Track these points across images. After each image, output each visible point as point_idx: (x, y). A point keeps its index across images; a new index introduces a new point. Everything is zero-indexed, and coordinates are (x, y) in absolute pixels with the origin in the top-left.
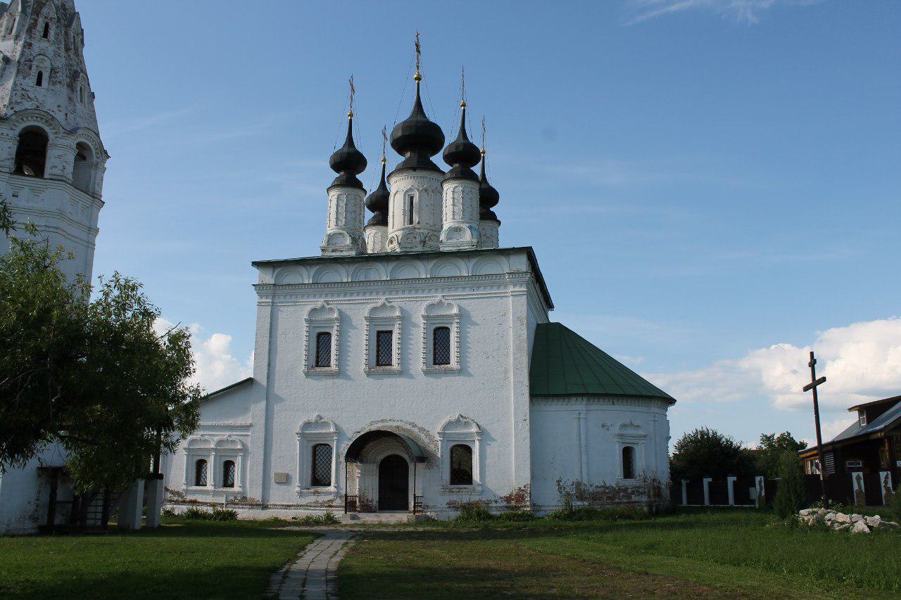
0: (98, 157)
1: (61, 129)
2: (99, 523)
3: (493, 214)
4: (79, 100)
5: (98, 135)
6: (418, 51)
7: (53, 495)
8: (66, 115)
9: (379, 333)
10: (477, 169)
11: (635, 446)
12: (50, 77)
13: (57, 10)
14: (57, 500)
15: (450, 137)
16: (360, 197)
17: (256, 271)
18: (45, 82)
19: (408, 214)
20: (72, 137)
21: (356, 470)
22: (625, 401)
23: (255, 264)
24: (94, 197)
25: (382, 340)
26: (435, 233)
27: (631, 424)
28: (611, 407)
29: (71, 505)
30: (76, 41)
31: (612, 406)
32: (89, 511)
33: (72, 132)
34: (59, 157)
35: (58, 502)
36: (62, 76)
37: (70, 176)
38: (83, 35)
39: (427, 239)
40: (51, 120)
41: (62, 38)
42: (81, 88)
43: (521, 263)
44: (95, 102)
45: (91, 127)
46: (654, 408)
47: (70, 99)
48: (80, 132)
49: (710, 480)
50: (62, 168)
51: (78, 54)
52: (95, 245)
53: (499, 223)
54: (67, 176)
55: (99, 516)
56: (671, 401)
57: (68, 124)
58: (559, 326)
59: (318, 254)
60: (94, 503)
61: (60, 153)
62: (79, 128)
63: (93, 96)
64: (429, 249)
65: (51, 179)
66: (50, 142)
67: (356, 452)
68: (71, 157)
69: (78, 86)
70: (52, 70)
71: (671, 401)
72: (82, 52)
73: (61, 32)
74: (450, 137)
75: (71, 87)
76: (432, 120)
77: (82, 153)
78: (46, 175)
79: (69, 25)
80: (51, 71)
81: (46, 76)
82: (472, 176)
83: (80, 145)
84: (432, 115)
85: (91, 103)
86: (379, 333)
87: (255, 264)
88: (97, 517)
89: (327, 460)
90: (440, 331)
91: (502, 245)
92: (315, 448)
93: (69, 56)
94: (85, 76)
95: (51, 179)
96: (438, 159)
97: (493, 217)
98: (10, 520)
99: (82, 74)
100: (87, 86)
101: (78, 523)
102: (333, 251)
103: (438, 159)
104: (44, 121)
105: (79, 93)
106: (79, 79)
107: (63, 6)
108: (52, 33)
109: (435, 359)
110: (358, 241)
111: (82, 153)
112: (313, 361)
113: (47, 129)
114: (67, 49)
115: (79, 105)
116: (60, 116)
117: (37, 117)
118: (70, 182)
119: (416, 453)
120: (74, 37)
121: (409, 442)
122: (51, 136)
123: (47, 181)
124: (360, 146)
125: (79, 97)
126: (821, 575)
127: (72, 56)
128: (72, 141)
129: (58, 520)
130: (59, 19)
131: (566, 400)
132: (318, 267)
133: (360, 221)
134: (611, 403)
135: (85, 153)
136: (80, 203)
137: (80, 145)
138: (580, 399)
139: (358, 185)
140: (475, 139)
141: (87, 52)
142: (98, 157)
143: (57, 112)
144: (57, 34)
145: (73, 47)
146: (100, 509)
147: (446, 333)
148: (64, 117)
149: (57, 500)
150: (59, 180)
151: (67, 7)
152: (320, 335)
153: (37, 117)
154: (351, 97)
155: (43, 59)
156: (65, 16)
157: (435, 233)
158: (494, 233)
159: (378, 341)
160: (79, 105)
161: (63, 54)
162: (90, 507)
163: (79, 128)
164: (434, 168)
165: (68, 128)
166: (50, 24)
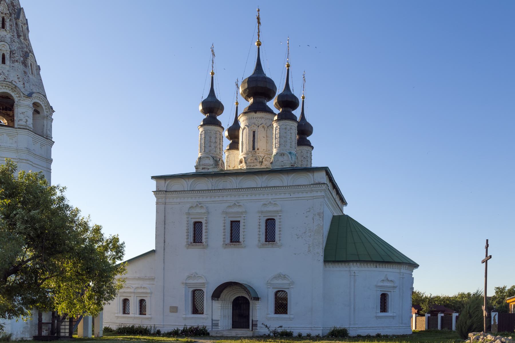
0: (47, 112)
1: (22, 94)
2: (67, 335)
3: (309, 141)
4: (31, 73)
5: (45, 96)
6: (259, 23)
7: (40, 319)
8: (24, 84)
9: (232, 222)
10: (297, 113)
11: (389, 293)
12: (10, 57)
13: (8, 7)
14: (42, 322)
15: (280, 90)
16: (220, 132)
17: (154, 182)
18: (7, 62)
19: (252, 143)
20: (29, 100)
21: (217, 305)
22: (384, 265)
23: (153, 178)
24: (47, 139)
25: (235, 226)
26: (269, 156)
27: (388, 280)
28: (375, 269)
29: (51, 325)
30: (24, 29)
31: (375, 268)
32: (61, 328)
33: (30, 95)
34: (23, 113)
35: (43, 323)
36: (18, 56)
37: (31, 126)
38: (27, 24)
39: (264, 160)
40: (15, 88)
41: (14, 28)
42: (31, 64)
43: (322, 177)
44: (41, 73)
45: (41, 91)
46: (404, 270)
47: (25, 72)
48: (34, 95)
49: (443, 315)
50: (25, 121)
51: (26, 39)
52: (51, 170)
53: (313, 148)
54: (30, 126)
55: (67, 331)
56: (416, 266)
57: (27, 90)
58: (347, 217)
59: (193, 170)
60: (63, 324)
61: (24, 110)
62: (33, 93)
63: (38, 68)
64: (265, 167)
65: (19, 128)
66: (16, 103)
67: (217, 295)
68: (30, 112)
69: (29, 61)
70: (11, 52)
71: (416, 266)
72: (28, 37)
73: (13, 24)
74: (280, 90)
75: (24, 63)
76: (268, 75)
77: (37, 109)
78: (16, 126)
79: (18, 18)
80: (10, 54)
81: (7, 56)
82: (293, 118)
83: (35, 104)
84: (269, 72)
85: (39, 74)
86: (232, 222)
87: (153, 178)
88: (66, 332)
89: (201, 302)
90: (270, 221)
91: (314, 165)
92: (194, 292)
93: (21, 41)
94: (33, 56)
95: (19, 128)
96: (272, 104)
97: (308, 144)
98: (17, 333)
99: (30, 54)
100: (34, 62)
101: (56, 335)
102: (203, 169)
103: (272, 104)
104: (10, 89)
105: (30, 67)
106: (29, 58)
107: (12, 3)
108: (7, 24)
109: (266, 239)
110: (217, 161)
111: (37, 109)
112: (191, 239)
113: (13, 94)
114: (19, 36)
115: (31, 76)
116: (20, 85)
117: (5, 86)
118: (32, 130)
119: (253, 295)
120: (22, 26)
121: (248, 288)
122: (16, 99)
123: (17, 129)
124: (220, 96)
125: (30, 70)
126: (319, 337)
127: (23, 41)
128: (29, 102)
129: (44, 333)
130: (11, 14)
131: (347, 264)
132: (193, 180)
133: (220, 148)
134: (375, 266)
135: (39, 109)
136: (39, 143)
137: (35, 104)
138: (355, 264)
139: (218, 124)
140: (297, 91)
141: (32, 37)
142: (47, 112)
143: (18, 82)
144: (11, 25)
145: (22, 35)
146: (68, 327)
147: (273, 222)
148: (22, 86)
149: (42, 322)
150: (24, 129)
151: (15, 4)
152: (195, 223)
153: (5, 86)
154: (213, 60)
155: (4, 44)
156: (15, 11)
157: (269, 156)
158: (309, 155)
159: (231, 227)
160: (31, 76)
161: (16, 40)
162: (61, 326)
163: (33, 93)
164: (270, 111)
165: (26, 93)
166: (5, 18)
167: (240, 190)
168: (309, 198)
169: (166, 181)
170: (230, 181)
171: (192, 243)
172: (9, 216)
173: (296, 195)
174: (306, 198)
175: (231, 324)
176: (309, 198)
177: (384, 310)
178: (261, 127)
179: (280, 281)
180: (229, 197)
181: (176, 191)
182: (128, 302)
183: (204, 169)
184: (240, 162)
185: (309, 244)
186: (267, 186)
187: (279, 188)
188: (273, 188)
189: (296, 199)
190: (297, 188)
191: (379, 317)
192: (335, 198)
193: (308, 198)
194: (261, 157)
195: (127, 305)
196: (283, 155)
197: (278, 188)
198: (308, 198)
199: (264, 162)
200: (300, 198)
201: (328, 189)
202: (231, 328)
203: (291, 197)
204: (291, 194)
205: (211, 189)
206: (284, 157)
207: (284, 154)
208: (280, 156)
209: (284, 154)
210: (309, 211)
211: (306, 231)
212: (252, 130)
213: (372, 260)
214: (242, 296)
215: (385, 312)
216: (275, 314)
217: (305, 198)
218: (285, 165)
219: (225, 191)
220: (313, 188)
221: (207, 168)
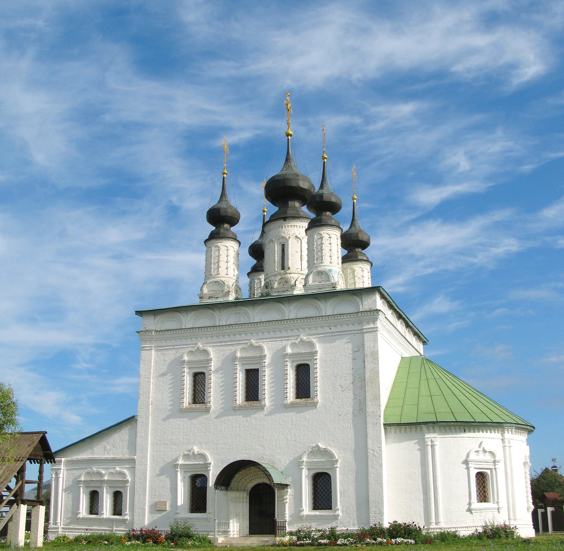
11: (488, 472)
23: (528, 513)
87: (528, 513)
167: (259, 325)
168: (357, 332)
169: (156, 317)
170: (245, 313)
171: (190, 403)
172: (88, 543)
173: (339, 328)
174: (353, 332)
175: (247, 528)
176: (357, 332)
177: (483, 499)
178: (293, 239)
179: (482, 456)
180: (243, 335)
181: (169, 330)
182: (96, 505)
183: (211, 298)
184: (265, 287)
185: (359, 400)
186: (296, 317)
187: (313, 319)
188: (305, 320)
189: (338, 333)
190: (339, 318)
191: (247, 340)
192: (404, 335)
193: (355, 332)
194: (293, 278)
195: (95, 509)
196: (320, 274)
197: (311, 319)
198: (355, 332)
199: (297, 286)
200: (344, 333)
201: (385, 317)
202: (248, 533)
203: (330, 331)
204: (331, 327)
205: (218, 325)
206: (322, 276)
207: (321, 273)
208: (317, 275)
209: (321, 273)
210: (358, 351)
211: (355, 381)
212: (280, 243)
213: (456, 420)
214: (264, 482)
215: (485, 501)
216: (313, 510)
217: (351, 332)
218: (324, 287)
219: (237, 327)
220: (362, 318)
221: (215, 297)
